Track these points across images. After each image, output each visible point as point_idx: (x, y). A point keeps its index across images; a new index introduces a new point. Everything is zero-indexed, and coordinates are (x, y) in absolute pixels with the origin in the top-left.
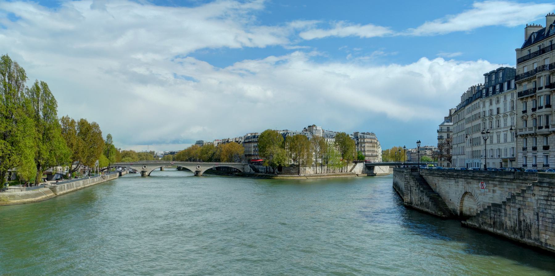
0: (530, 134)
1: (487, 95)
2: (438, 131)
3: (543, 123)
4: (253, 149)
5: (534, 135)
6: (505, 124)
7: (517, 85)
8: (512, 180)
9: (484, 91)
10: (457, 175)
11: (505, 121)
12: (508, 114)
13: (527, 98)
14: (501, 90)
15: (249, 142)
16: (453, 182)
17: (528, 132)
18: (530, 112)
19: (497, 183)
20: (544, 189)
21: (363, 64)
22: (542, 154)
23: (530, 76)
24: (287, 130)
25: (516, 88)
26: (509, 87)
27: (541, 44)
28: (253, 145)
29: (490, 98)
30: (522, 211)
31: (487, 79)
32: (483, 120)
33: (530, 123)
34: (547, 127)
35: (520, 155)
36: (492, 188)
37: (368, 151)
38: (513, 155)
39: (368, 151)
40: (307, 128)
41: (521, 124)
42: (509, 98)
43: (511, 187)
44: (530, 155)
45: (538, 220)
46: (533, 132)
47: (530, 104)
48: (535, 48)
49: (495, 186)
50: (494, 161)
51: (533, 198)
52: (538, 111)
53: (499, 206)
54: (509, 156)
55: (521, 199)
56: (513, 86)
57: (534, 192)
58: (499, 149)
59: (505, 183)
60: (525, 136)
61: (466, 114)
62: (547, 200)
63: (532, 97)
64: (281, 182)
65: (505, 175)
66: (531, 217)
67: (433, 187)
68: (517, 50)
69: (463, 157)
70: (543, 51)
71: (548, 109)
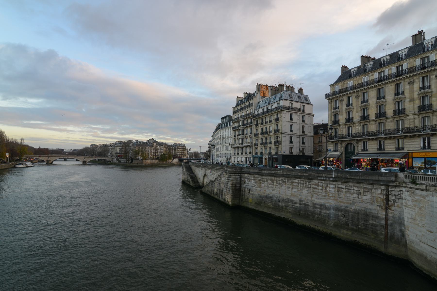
4: (119, 150)
11: (228, 140)
14: (227, 126)
15: (117, 146)
16: (200, 170)
17: (247, 145)
21: (8, 125)
23: (237, 121)
28: (119, 148)
33: (237, 142)
42: (230, 130)
46: (249, 144)
49: (214, 171)
54: (229, 157)
55: (219, 178)
67: (194, 172)
68: (233, 108)
70: (242, 109)
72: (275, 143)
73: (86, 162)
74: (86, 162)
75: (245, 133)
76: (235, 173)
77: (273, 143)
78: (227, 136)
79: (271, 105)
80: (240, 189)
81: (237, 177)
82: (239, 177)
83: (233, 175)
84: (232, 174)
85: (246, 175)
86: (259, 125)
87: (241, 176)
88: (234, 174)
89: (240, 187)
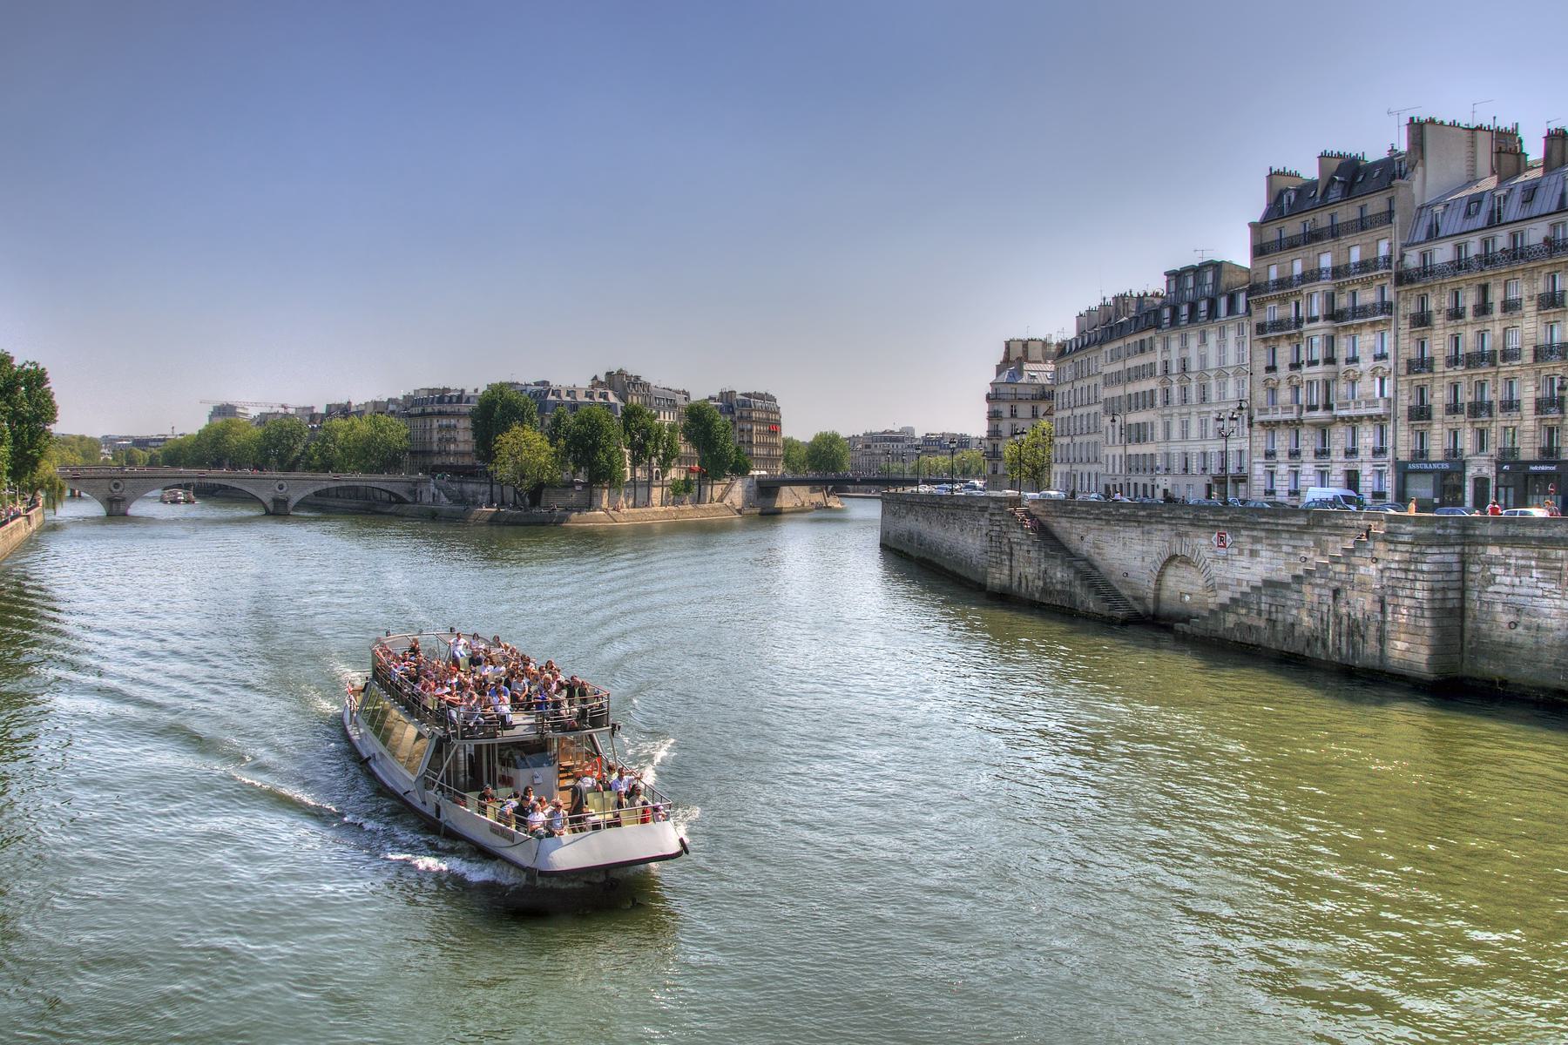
0: (1286, 422)
1: (1174, 321)
2: (988, 398)
3: (1318, 397)
5: (1295, 425)
6: (1222, 396)
7: (1253, 307)
8: (1302, 530)
9: (1166, 313)
10: (1149, 516)
12: (1230, 372)
13: (1278, 338)
14: (1213, 312)
15: (423, 414)
16: (1133, 533)
17: (1279, 416)
18: (1283, 371)
19: (1263, 534)
20: (1400, 547)
22: (1312, 466)
24: (545, 383)
25: (1248, 311)
26: (1231, 309)
27: (1310, 218)
29: (1183, 331)
30: (1343, 595)
31: (1173, 284)
32: (1162, 383)
33: (1285, 395)
34: (1328, 407)
35: (1259, 470)
36: (1249, 547)
37: (759, 445)
38: (1240, 468)
39: (759, 445)
40: (602, 378)
41: (1261, 396)
43: (1298, 543)
44: (1283, 469)
45: (1383, 611)
47: (1285, 353)
48: (1293, 227)
49: (1256, 540)
50: (1190, 480)
51: (1373, 566)
52: (1305, 369)
53: (1284, 585)
56: (1242, 307)
57: (1376, 554)
58: (1205, 454)
59: (1285, 535)
60: (1271, 426)
61: (1104, 362)
62: (1406, 571)
63: (1289, 337)
64: (597, 542)
65: (1284, 517)
66: (1367, 607)
69: (1094, 468)
71: (1330, 368)
72: (1541, 406)
73: (285, 502)
74: (285, 502)
75: (1343, 351)
76: (1443, 541)
77: (1528, 406)
78: (1213, 363)
79: (1513, 228)
80: (1463, 609)
81: (1449, 558)
82: (1455, 558)
83: (1435, 550)
84: (1430, 546)
85: (1493, 551)
86: (1438, 320)
87: (1462, 554)
88: (1439, 545)
89: (1463, 599)
